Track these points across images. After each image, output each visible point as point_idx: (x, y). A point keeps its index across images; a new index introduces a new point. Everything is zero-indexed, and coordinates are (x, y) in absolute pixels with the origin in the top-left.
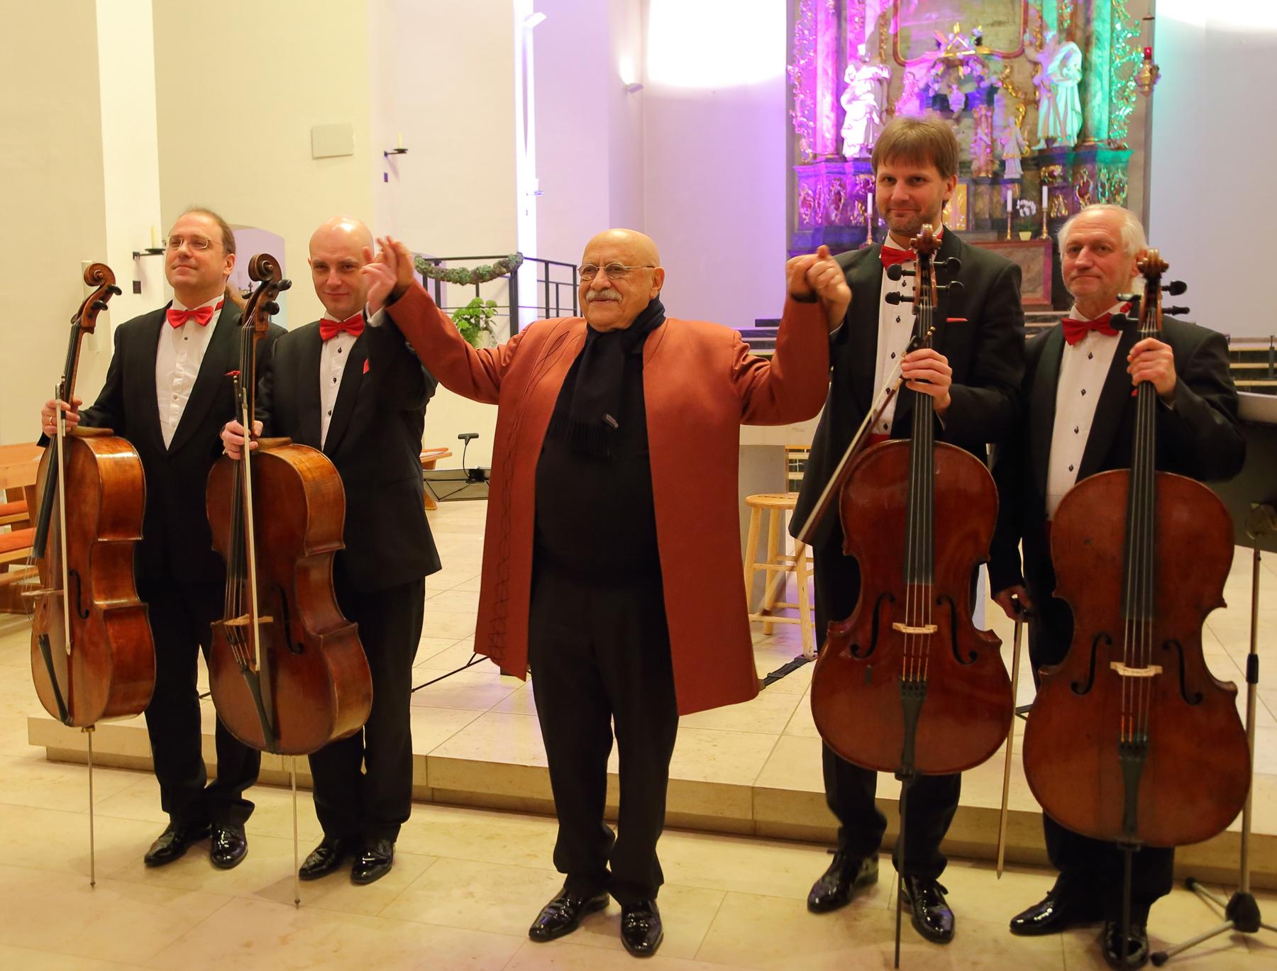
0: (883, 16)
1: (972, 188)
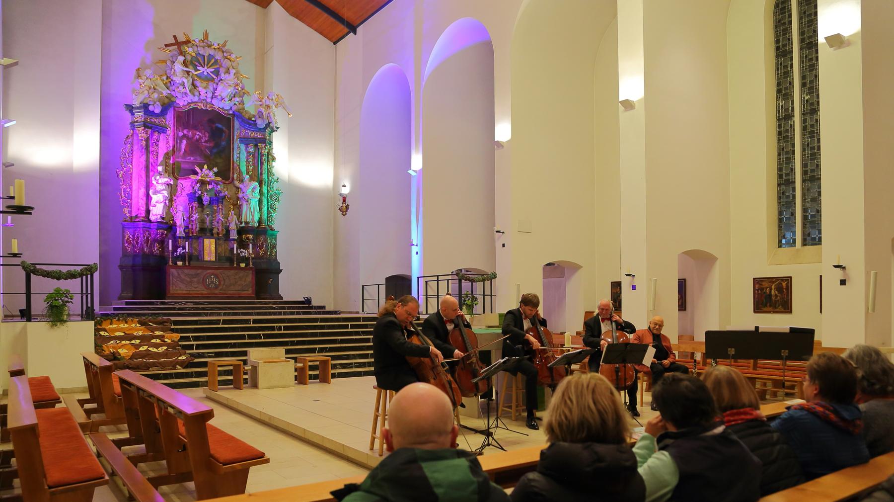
0: (167, 154)
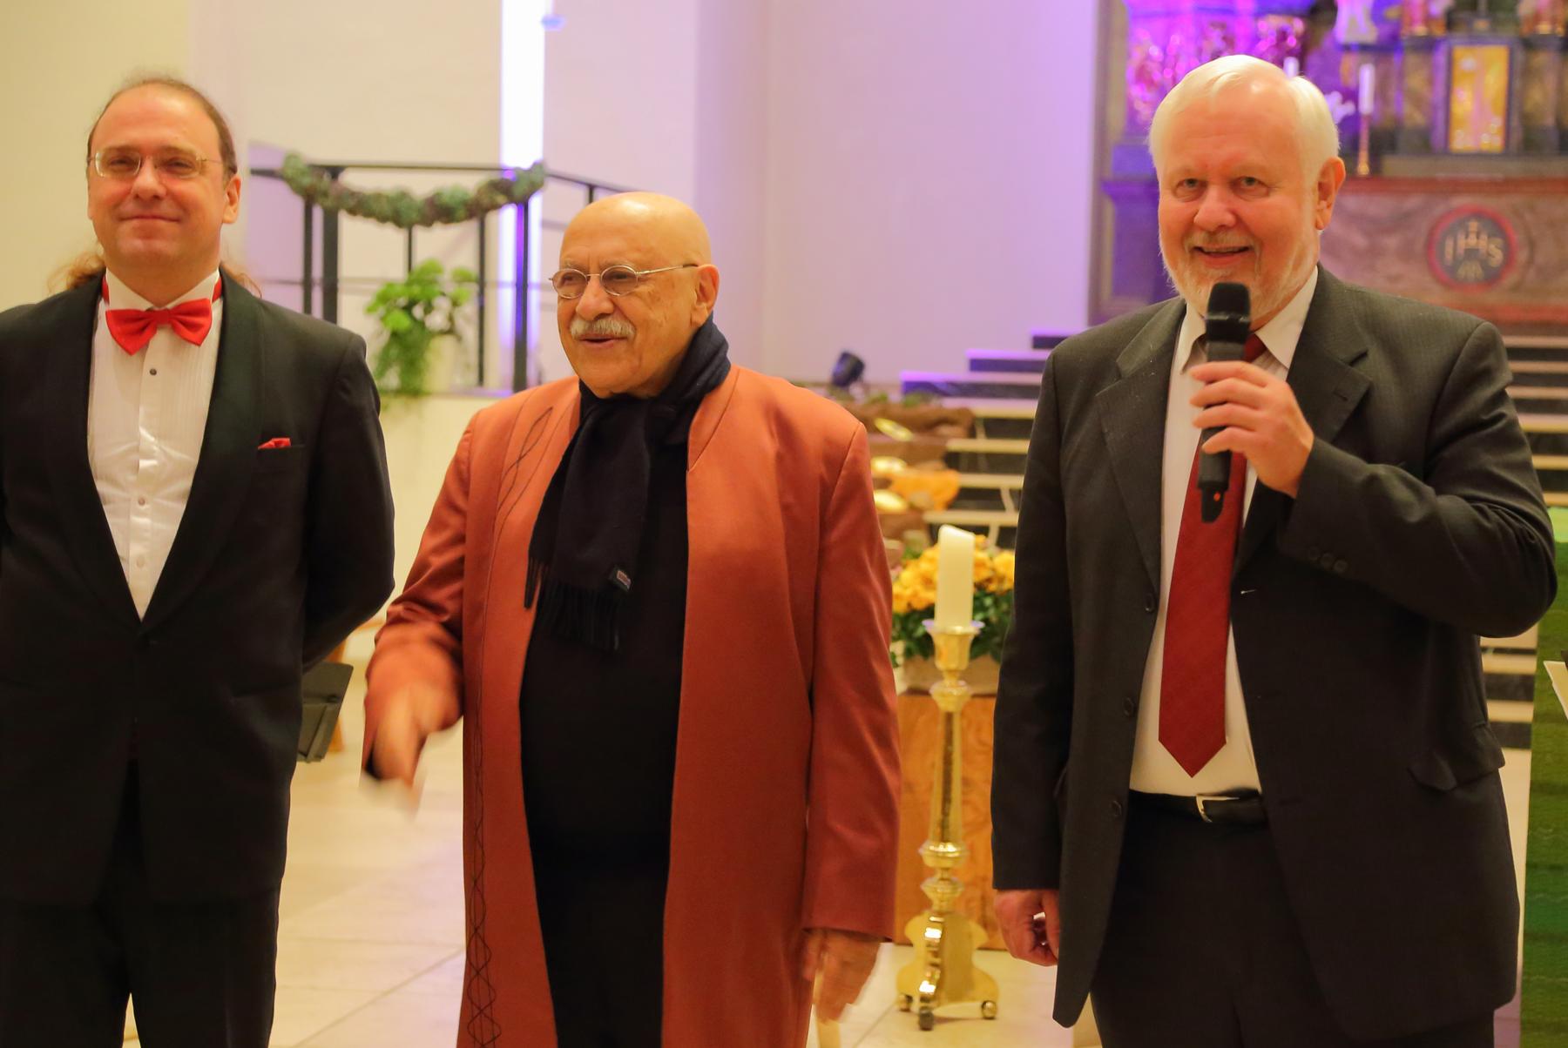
1: (1520, 56)
